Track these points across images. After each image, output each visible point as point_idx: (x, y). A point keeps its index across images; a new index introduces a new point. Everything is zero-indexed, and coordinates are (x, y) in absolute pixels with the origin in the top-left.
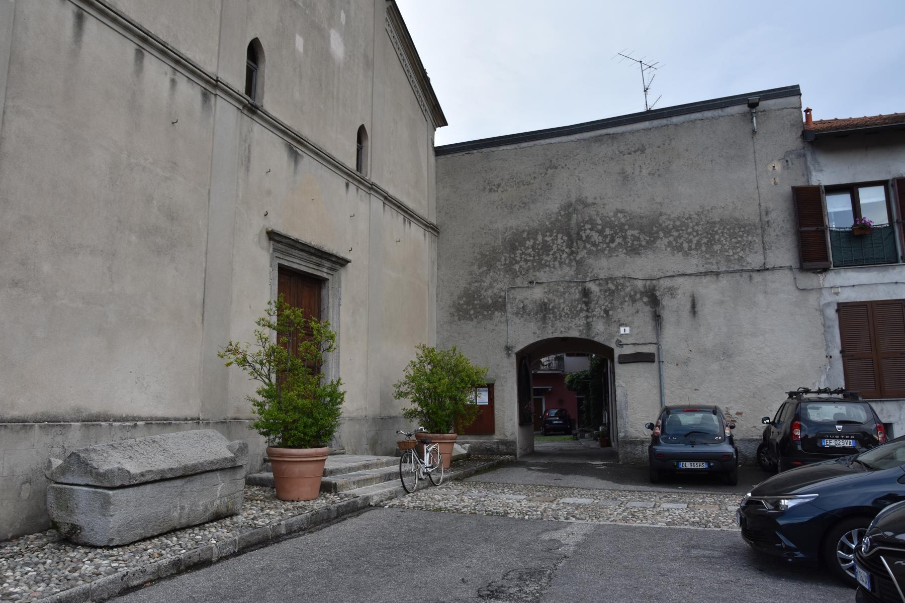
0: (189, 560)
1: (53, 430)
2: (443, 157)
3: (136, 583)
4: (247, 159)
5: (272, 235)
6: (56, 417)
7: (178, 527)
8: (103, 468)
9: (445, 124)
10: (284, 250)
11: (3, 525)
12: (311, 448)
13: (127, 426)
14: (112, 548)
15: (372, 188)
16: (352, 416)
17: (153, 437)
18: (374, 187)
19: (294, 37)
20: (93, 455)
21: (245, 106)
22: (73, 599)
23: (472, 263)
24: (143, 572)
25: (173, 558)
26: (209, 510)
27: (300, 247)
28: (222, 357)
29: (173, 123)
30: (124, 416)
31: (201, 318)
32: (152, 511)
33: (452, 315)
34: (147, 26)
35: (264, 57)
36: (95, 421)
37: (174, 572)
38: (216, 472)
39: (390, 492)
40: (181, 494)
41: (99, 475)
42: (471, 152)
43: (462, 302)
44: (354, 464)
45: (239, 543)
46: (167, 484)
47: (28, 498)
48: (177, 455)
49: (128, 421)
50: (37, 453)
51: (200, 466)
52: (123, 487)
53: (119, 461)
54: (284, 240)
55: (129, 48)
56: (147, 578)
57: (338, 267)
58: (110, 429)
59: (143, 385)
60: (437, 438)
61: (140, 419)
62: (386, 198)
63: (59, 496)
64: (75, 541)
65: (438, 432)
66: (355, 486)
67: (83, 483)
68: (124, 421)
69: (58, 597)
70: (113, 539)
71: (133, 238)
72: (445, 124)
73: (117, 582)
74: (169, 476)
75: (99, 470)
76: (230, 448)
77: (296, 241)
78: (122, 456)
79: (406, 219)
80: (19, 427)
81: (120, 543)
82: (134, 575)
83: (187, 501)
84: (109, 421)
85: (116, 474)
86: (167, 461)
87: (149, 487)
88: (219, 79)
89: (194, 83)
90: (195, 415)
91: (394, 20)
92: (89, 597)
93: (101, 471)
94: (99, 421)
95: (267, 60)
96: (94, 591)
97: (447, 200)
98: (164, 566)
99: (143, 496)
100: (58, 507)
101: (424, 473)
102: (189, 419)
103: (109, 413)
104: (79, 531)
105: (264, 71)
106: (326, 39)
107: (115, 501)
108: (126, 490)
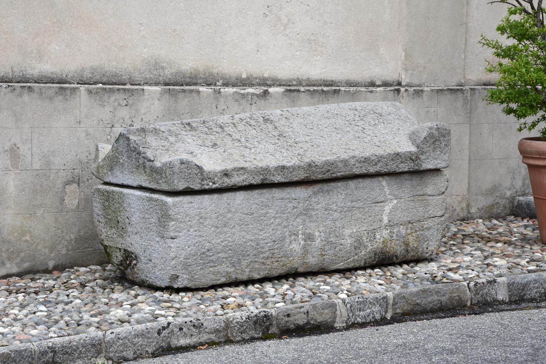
1: (113, 98)
3: (183, 342)
6: (116, 75)
7: (301, 270)
11: (39, 248)
13: (248, 94)
14: (178, 291)
17: (268, 112)
20: (151, 140)
24: (198, 326)
25: (256, 312)
32: (248, 237)
36: (188, 84)
37: (256, 336)
38: (380, 179)
40: (306, 212)
41: (156, 172)
45: (393, 305)
46: (277, 193)
47: (78, 207)
48: (300, 145)
49: (251, 85)
51: (340, 165)
52: (188, 192)
53: (192, 149)
56: (204, 338)
58: (216, 99)
59: (279, 19)
63: (107, 204)
64: (130, 277)
67: (135, 184)
69: (50, 344)
70: (178, 277)
74: (278, 179)
75: (155, 163)
76: (412, 137)
78: (200, 142)
80: (53, 90)
81: (190, 285)
82: (181, 329)
83: (318, 226)
84: (215, 85)
85: (176, 169)
86: (278, 155)
87: (240, 196)
90: (390, 75)
92: (101, 352)
93: (158, 164)
94: (196, 84)
96: (110, 344)
98: (237, 322)
99: (230, 211)
100: (106, 222)
102: (378, 83)
103: (215, 71)
104: (135, 262)
107: (178, 214)
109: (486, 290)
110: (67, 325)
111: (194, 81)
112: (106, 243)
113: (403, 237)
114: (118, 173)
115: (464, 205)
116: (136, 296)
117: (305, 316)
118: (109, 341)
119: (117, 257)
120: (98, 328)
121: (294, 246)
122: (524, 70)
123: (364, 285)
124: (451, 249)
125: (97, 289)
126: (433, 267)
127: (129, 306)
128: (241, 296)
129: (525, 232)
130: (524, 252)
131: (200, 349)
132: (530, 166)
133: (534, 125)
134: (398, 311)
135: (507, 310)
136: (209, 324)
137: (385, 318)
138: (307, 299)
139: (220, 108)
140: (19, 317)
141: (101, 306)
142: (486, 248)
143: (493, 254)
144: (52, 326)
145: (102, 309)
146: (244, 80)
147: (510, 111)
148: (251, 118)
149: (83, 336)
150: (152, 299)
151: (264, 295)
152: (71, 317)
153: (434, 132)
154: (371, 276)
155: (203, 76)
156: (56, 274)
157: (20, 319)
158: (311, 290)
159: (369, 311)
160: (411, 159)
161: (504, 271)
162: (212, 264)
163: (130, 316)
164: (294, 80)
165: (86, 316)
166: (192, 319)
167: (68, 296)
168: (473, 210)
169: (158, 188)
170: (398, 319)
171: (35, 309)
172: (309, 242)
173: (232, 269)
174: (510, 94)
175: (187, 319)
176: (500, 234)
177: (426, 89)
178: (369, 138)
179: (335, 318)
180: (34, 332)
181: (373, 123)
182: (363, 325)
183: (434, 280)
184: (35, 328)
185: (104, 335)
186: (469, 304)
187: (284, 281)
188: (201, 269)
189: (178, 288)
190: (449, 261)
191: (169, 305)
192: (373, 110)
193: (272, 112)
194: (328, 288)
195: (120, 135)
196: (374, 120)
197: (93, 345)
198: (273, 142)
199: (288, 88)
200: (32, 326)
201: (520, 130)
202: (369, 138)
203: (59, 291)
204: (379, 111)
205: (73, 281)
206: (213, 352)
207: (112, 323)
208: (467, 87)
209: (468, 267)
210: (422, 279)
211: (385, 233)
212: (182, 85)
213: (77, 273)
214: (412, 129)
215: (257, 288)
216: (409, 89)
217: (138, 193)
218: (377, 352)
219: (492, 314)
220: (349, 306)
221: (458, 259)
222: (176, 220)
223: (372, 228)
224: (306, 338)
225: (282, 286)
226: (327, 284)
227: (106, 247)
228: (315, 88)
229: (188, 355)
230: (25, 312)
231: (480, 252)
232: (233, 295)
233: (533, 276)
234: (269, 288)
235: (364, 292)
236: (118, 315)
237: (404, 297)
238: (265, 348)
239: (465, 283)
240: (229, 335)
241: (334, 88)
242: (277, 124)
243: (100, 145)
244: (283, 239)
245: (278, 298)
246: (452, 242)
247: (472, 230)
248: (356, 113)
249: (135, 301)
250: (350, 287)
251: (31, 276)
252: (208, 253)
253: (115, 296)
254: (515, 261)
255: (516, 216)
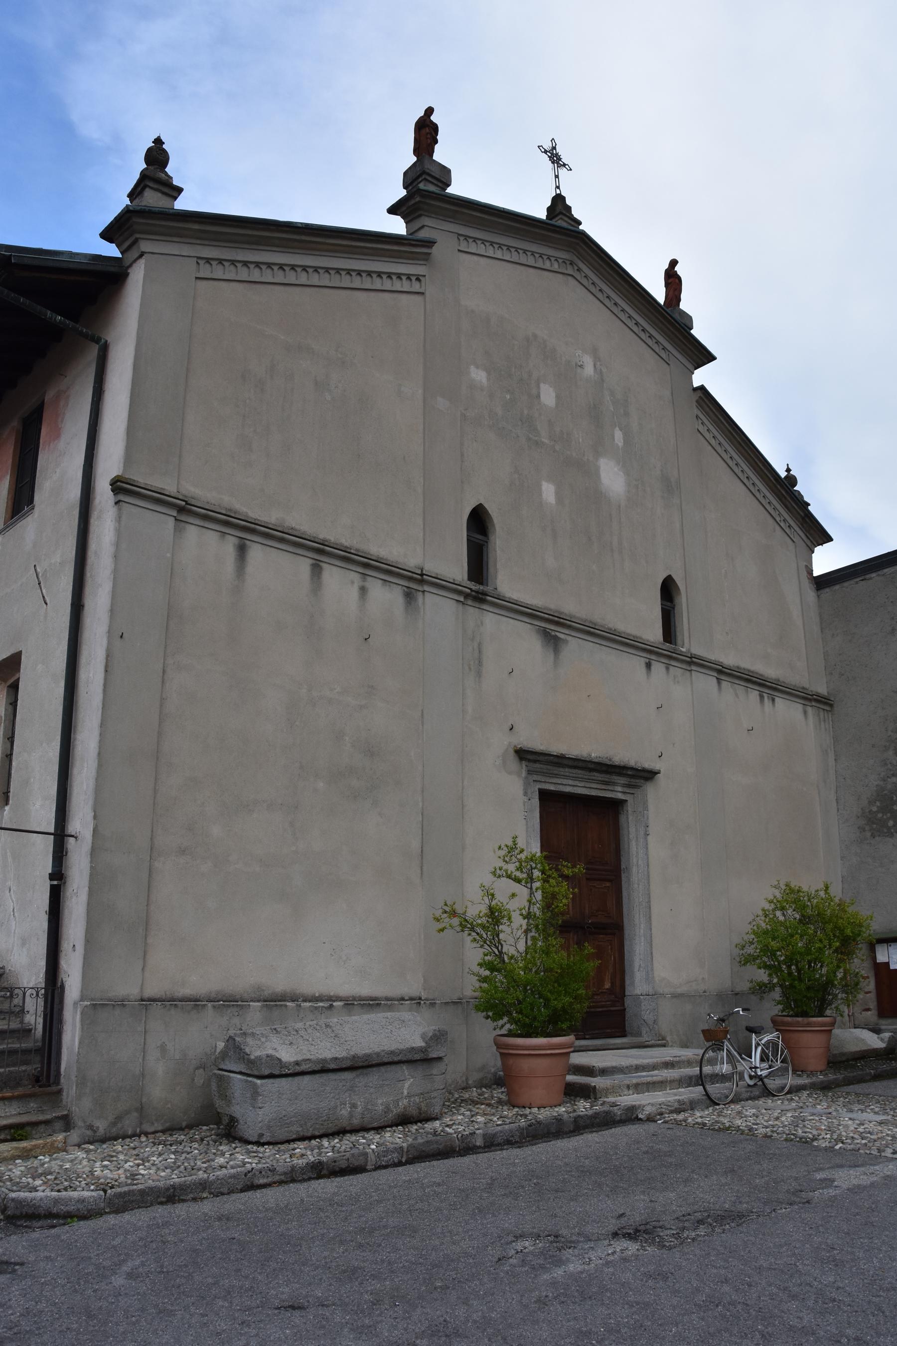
0: (333, 1164)
1: (229, 1011)
2: (827, 590)
3: (262, 1181)
4: (477, 662)
5: (523, 754)
7: (348, 1128)
8: (255, 1053)
9: (828, 539)
10: (545, 771)
12: (545, 1037)
13: (319, 1007)
14: (263, 1144)
15: (693, 662)
16: (679, 991)
18: (694, 659)
19: (539, 486)
20: (249, 1040)
21: (467, 596)
22: (189, 1188)
23: (885, 746)
24: (273, 1170)
25: (313, 1159)
26: (392, 1111)
27: (570, 763)
28: (438, 920)
29: (366, 639)
30: (317, 995)
31: (419, 871)
32: (312, 1106)
33: (862, 829)
34: (322, 535)
35: (493, 525)
37: (313, 1176)
38: (402, 1065)
39: (679, 1101)
40: (352, 1089)
41: (251, 1063)
42: (867, 576)
43: (874, 809)
44: (646, 1061)
45: (407, 1152)
46: (332, 1076)
47: (203, 1084)
48: (348, 1043)
49: (322, 1001)
50: (211, 1035)
52: (271, 1076)
53: (275, 1047)
54: (541, 758)
55: (303, 565)
56: (277, 1178)
57: (639, 782)
60: (798, 1024)
61: (339, 999)
62: (719, 672)
65: (805, 1014)
66: (631, 1092)
67: (238, 1070)
68: (317, 1001)
69: (172, 1183)
70: (263, 1135)
71: (321, 785)
72: (828, 539)
73: (239, 1177)
74: (332, 1066)
76: (423, 1036)
77: (562, 757)
78: (281, 1042)
79: (764, 694)
82: (261, 1172)
84: (298, 1001)
85: (263, 1061)
87: (307, 1078)
88: (424, 572)
89: (391, 584)
90: (414, 993)
91: (711, 413)
93: (252, 1057)
94: (285, 1001)
95: (497, 529)
96: (212, 1183)
97: (840, 655)
99: (299, 1089)
101: (751, 1077)
102: (406, 998)
103: (298, 992)
104: (236, 1124)
105: (495, 543)
106: (594, 474)
107: (264, 1091)
108: (278, 1081)
109: (469, 1140)
110: (185, 1170)
111: (284, 999)
112: (219, 1110)
113: (418, 1104)
114: (227, 1063)
115: (464, 1079)
116: (235, 1149)
117: (346, 1162)
118: (211, 1181)
119: (225, 1120)
120: (205, 1171)
121: (344, 1112)
122: (493, 992)
123: (388, 1138)
124: (451, 1111)
125: (211, 1142)
126: (437, 1124)
127: (229, 1156)
128: (305, 1148)
129: (501, 1097)
130: (497, 1111)
131: (273, 1186)
132: (501, 1054)
133: (502, 1026)
134: (410, 1156)
135: (482, 1153)
136: (280, 1169)
137: (401, 1161)
138: (349, 1150)
139: (300, 1016)
140: (156, 1163)
141: (210, 1155)
142: (474, 1109)
143: (478, 1113)
144: (175, 1170)
145: (211, 1158)
146: (317, 997)
147: (487, 1017)
148: (317, 1025)
149: (194, 1177)
150: (245, 1151)
151: (320, 1147)
152: (189, 1163)
153: (437, 1033)
154: (395, 1132)
155: (289, 995)
156: (186, 1131)
157: (157, 1164)
158: (352, 1143)
159: (390, 1157)
160: (422, 1051)
161: (482, 1125)
162: (287, 1126)
163: (228, 1163)
164: (351, 997)
165: (199, 1163)
166: (268, 1165)
167: (191, 1147)
168: (470, 1082)
169: (252, 1073)
170: (410, 1162)
171: (167, 1157)
172: (353, 1109)
173: (301, 1129)
174: (487, 1007)
175: (265, 1166)
176: (485, 1098)
177: (437, 1002)
178: (395, 1037)
179: (367, 1162)
180: (163, 1174)
181: (398, 1027)
182: (385, 1167)
183: (435, 1133)
184: (164, 1172)
185: (208, 1177)
186: (457, 1149)
187: (336, 1136)
188: (280, 1129)
189: (263, 1143)
190: (448, 1119)
191: (256, 1154)
192: (398, 1018)
193: (330, 1020)
194: (364, 1141)
195: (230, 1037)
196: (399, 1025)
197: (201, 1184)
198: (330, 1041)
199: (346, 1002)
200: (162, 1169)
201: (495, 1029)
202: (395, 1037)
203: (186, 1144)
204: (403, 1018)
205: (196, 1136)
206: (281, 1189)
207: (215, 1168)
208: (464, 1000)
209: (459, 1124)
210: (428, 1133)
211: (405, 1101)
212: (275, 1001)
213: (200, 1131)
214: (423, 1030)
215: (317, 1142)
216: (427, 1002)
217: (239, 1076)
218: (390, 1187)
219: (471, 1156)
220: (376, 1154)
221: (455, 1118)
222: (263, 1095)
223: (396, 1098)
224: (346, 1178)
225: (334, 1140)
226: (364, 1138)
227: (218, 1113)
228: (365, 1002)
229: (264, 1190)
230: (160, 1159)
231: (469, 1112)
232: (300, 1147)
233: (499, 1128)
234: (325, 1142)
235: (388, 1144)
236: (220, 1162)
237: (414, 1146)
238: (317, 1185)
239: (455, 1135)
240: (294, 1176)
241: (377, 1002)
242: (334, 1029)
243: (218, 1043)
244: (336, 1107)
245: (329, 1150)
246: (453, 1105)
247: (468, 1096)
248: (387, 1020)
249: (234, 1151)
250: (379, 1140)
251: (170, 1132)
252: (284, 1118)
253: (221, 1148)
254: (490, 1118)
255: (498, 1085)
